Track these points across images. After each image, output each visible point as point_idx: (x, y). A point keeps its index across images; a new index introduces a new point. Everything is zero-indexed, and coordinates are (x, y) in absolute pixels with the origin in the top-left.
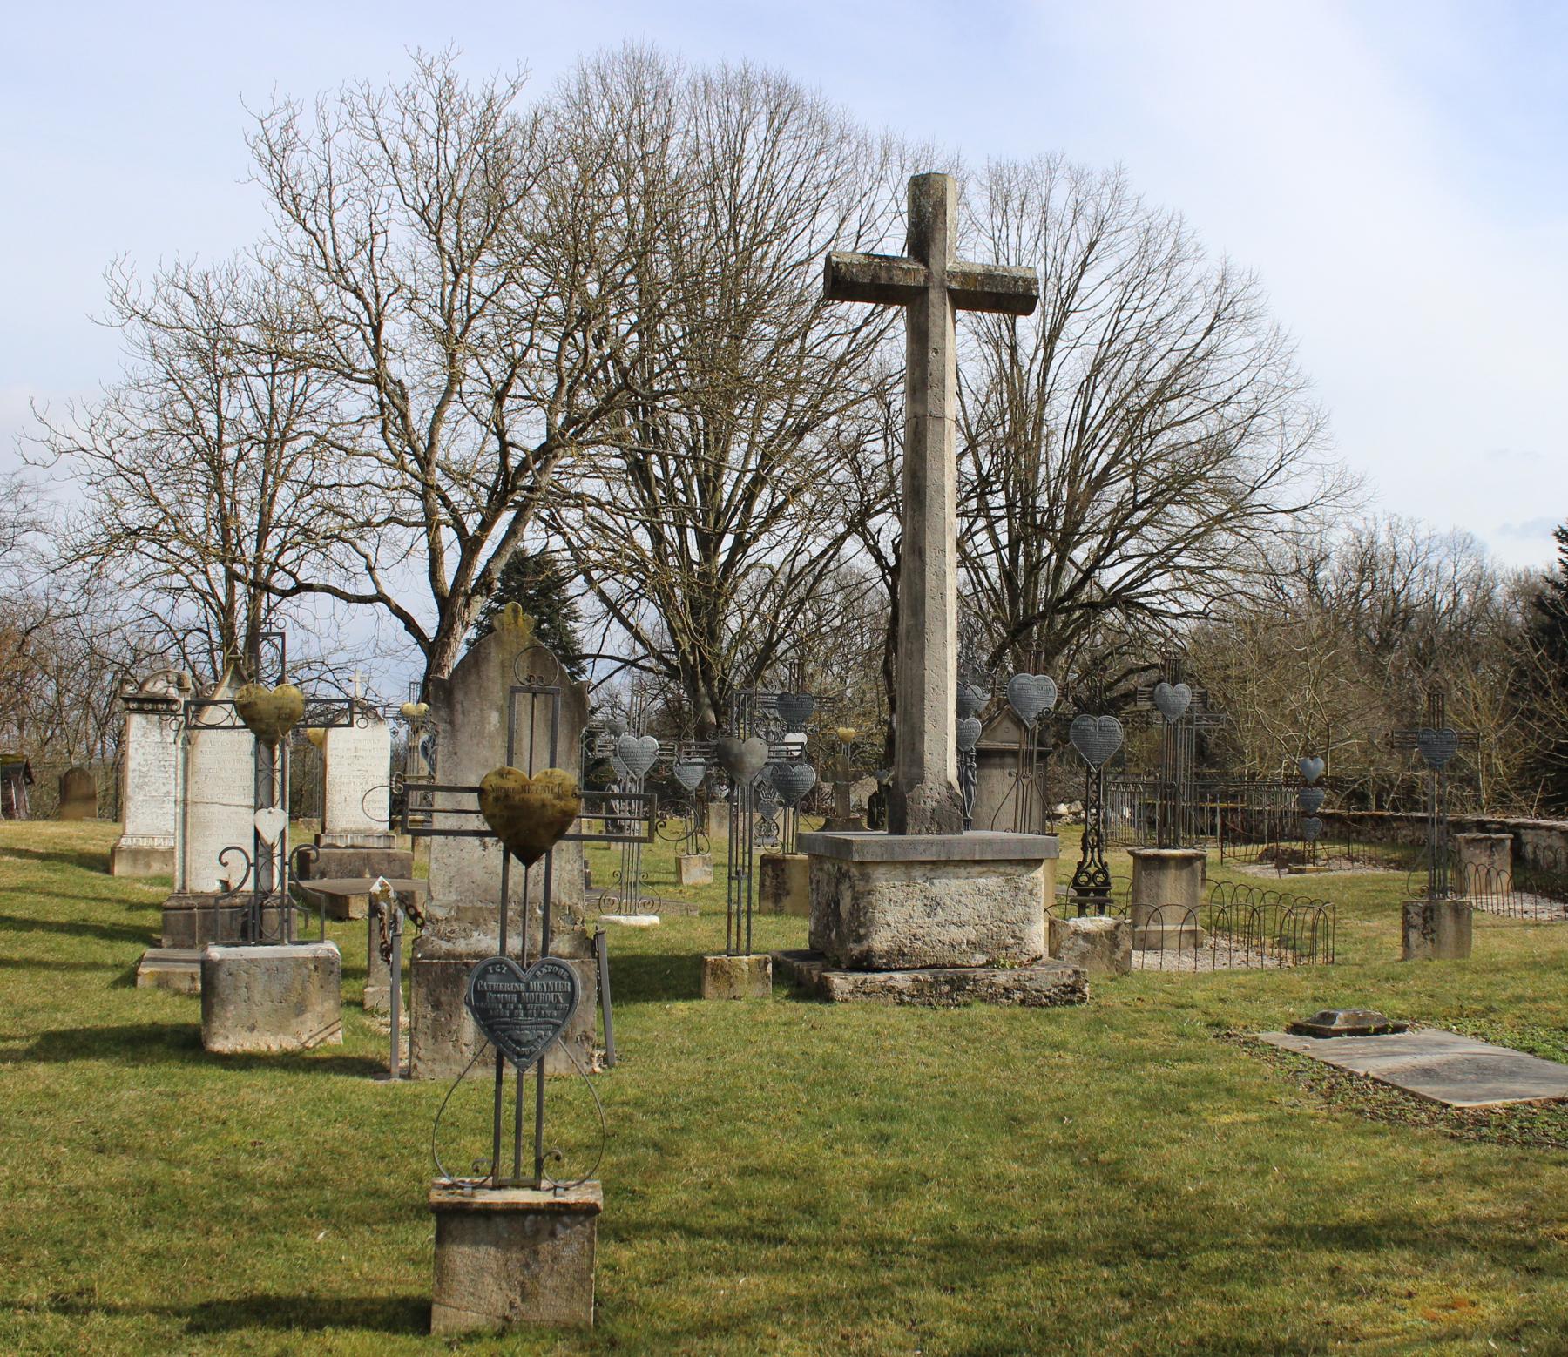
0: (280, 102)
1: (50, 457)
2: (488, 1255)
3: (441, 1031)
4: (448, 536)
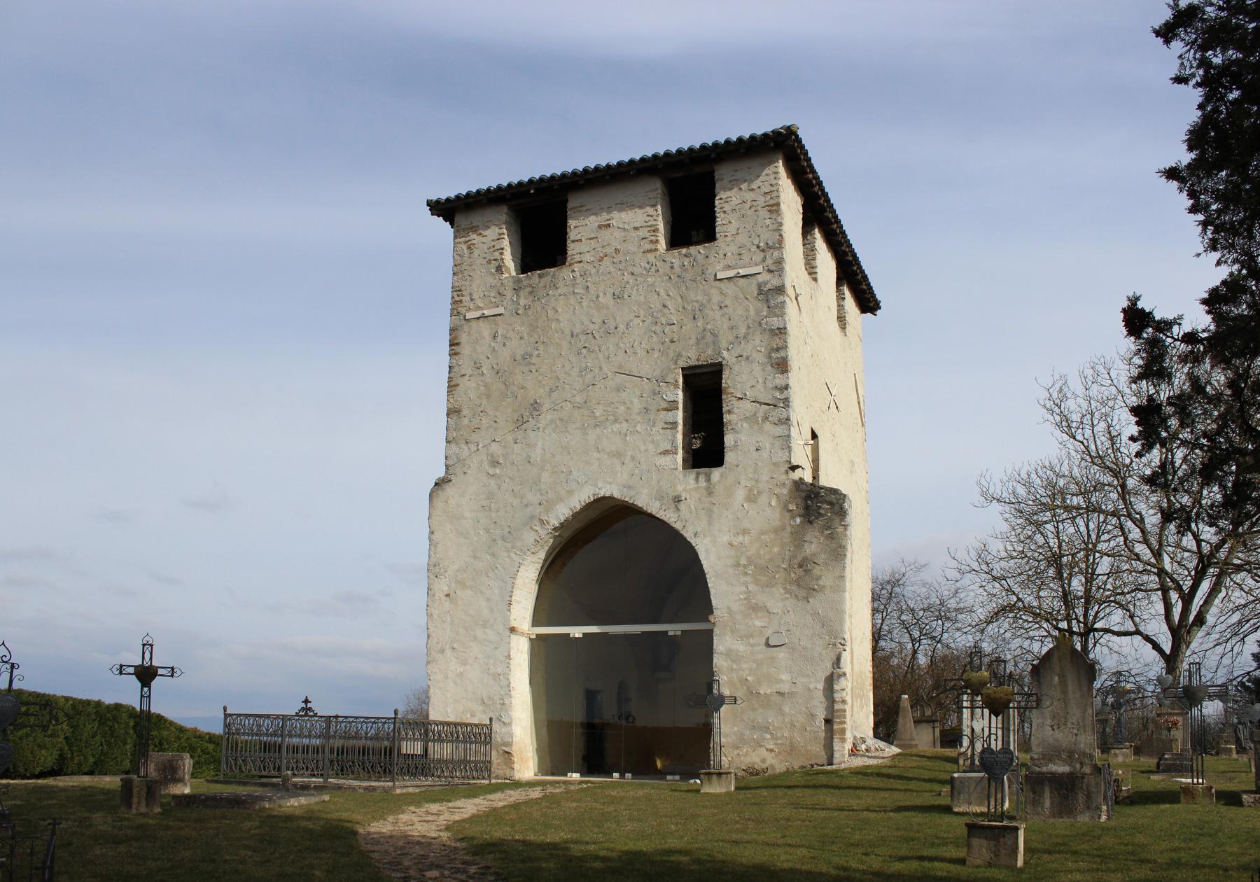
0: (1057, 377)
1: (959, 576)
2: (984, 842)
3: (1036, 803)
4: (1174, 596)
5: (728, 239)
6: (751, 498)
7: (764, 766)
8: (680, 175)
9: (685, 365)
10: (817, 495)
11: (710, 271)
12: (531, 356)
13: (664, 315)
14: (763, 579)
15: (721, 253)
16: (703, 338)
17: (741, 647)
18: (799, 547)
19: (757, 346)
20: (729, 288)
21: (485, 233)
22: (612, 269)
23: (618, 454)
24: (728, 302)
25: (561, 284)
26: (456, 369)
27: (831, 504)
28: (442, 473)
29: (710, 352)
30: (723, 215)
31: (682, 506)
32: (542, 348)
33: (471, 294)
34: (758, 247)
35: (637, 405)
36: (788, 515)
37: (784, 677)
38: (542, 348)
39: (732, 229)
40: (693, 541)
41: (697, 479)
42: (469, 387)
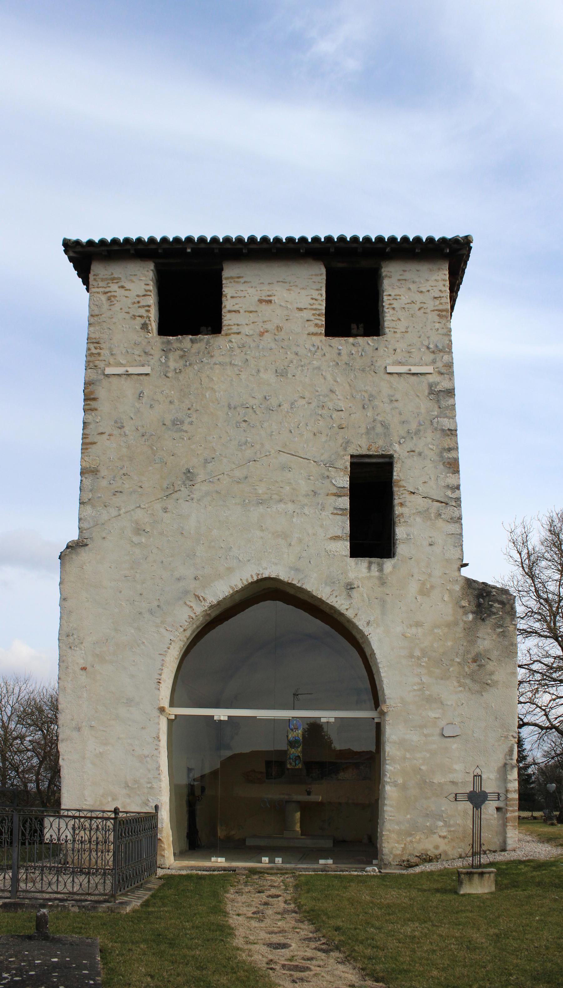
5: (398, 335)
6: (424, 592)
7: (437, 852)
8: (340, 265)
9: (356, 453)
10: (489, 593)
11: (380, 363)
12: (182, 422)
13: (332, 400)
14: (437, 671)
15: (391, 347)
16: (373, 428)
17: (414, 737)
18: (472, 642)
19: (428, 442)
20: (401, 384)
21: (128, 285)
22: (273, 345)
23: (284, 535)
24: (398, 396)
25: (216, 353)
26: (92, 426)
27: (502, 603)
28: (75, 536)
29: (381, 443)
30: (391, 311)
31: (354, 593)
32: (194, 416)
33: (111, 349)
34: (428, 348)
35: (304, 487)
36: (461, 611)
37: (456, 767)
38: (194, 416)
39: (401, 326)
40: (366, 630)
41: (369, 568)
42: (108, 449)
